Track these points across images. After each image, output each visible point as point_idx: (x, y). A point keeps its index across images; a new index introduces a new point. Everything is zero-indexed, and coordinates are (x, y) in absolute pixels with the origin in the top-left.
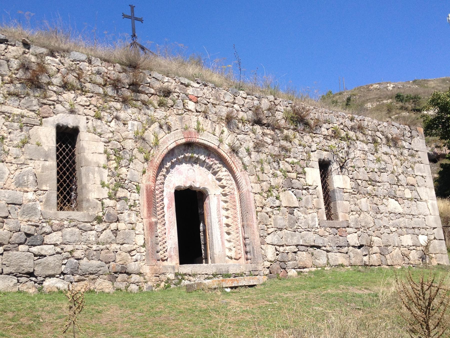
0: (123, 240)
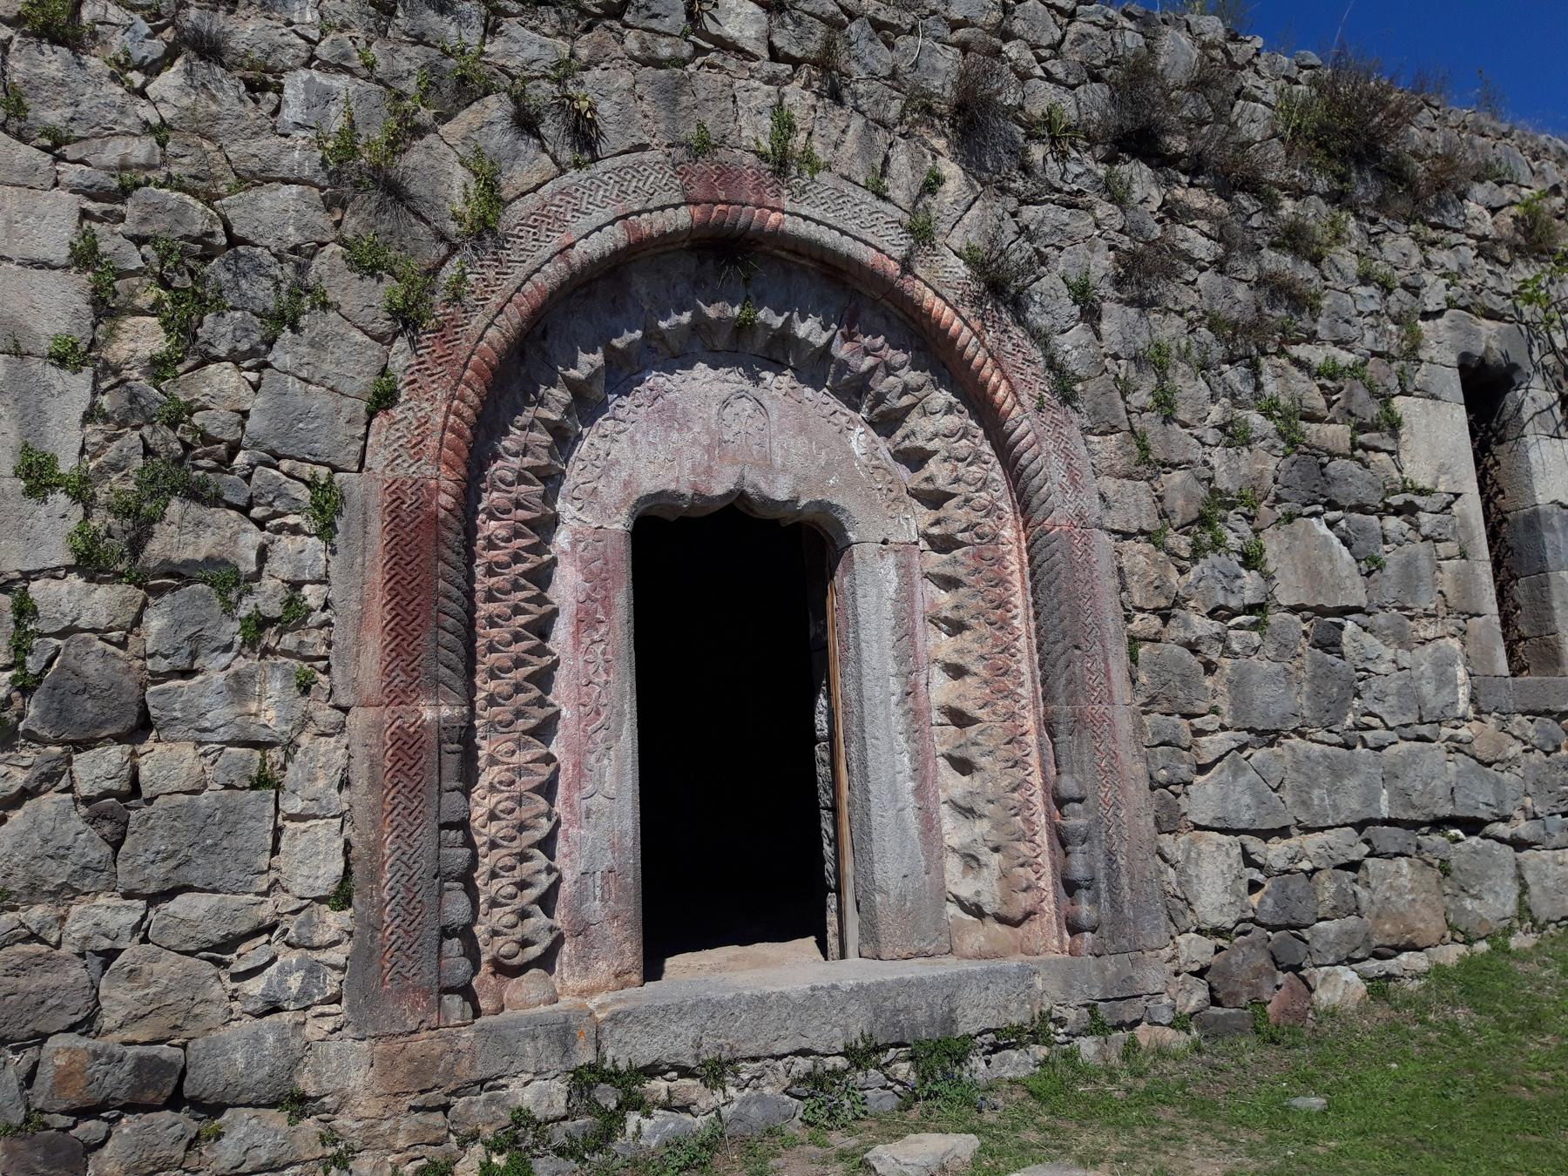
0: (172, 863)
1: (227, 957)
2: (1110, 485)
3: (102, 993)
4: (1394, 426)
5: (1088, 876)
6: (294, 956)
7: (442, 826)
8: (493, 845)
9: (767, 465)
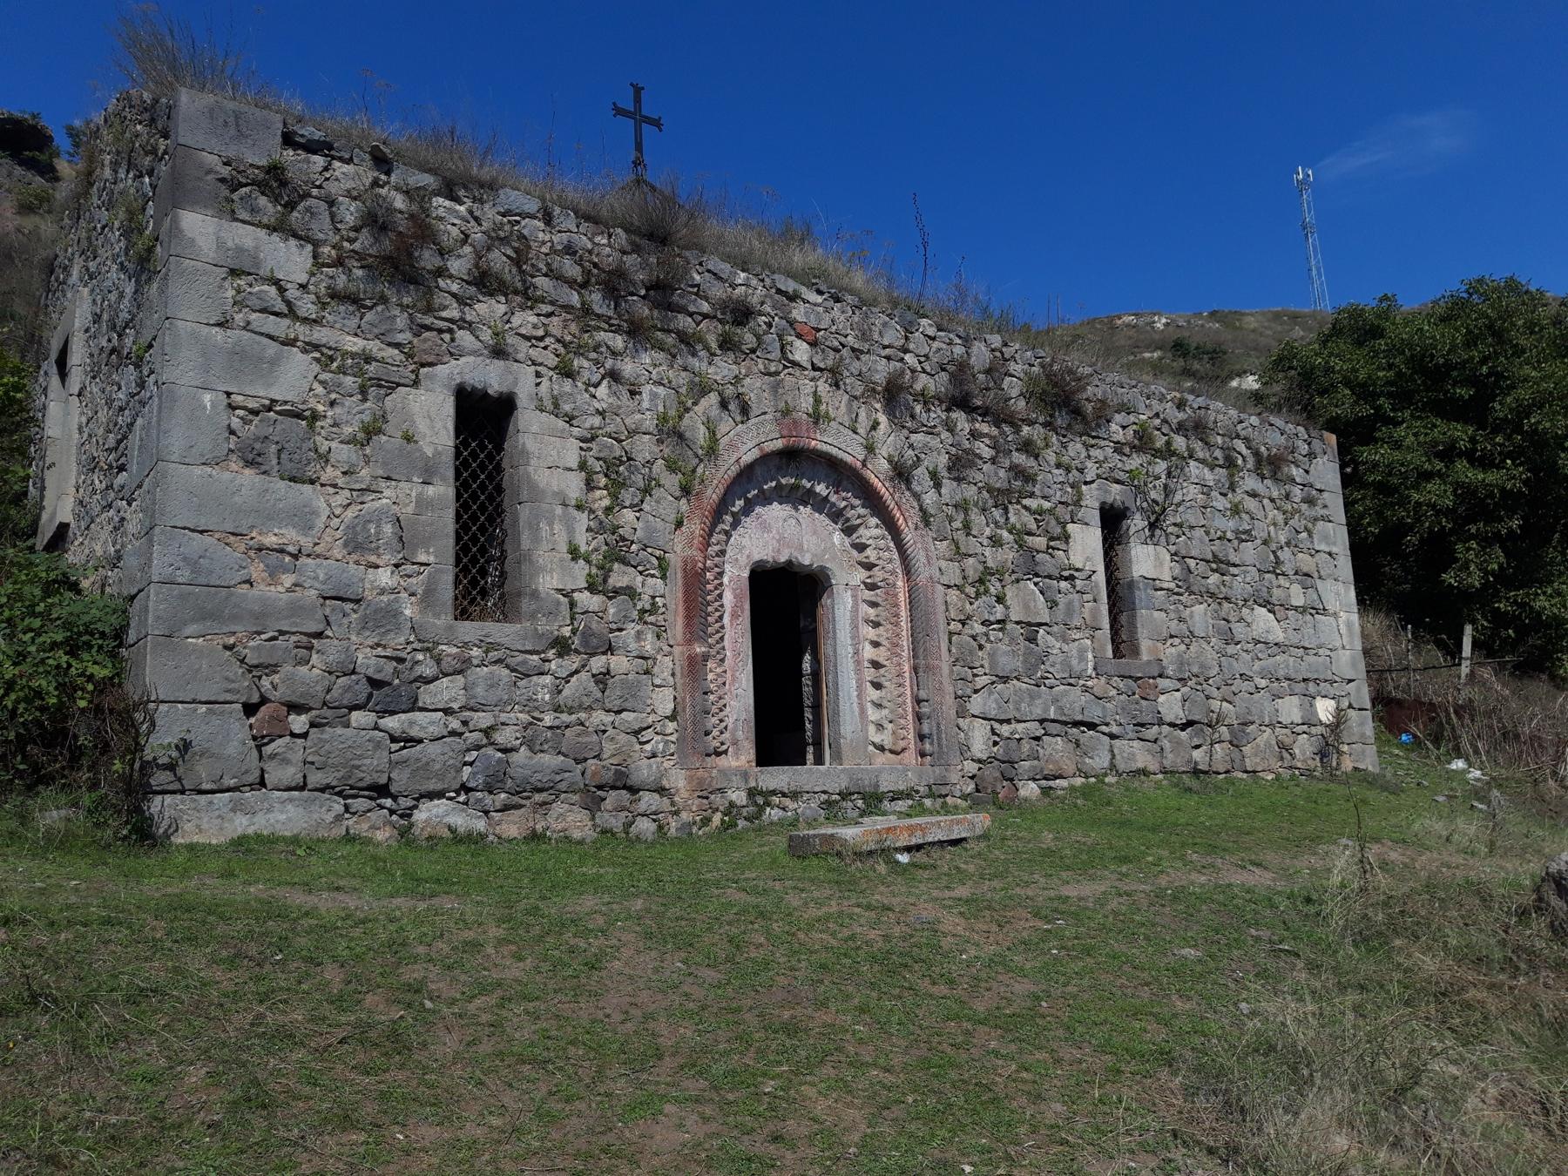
2: (943, 564)
4: (1066, 538)
6: (659, 737)
9: (801, 548)
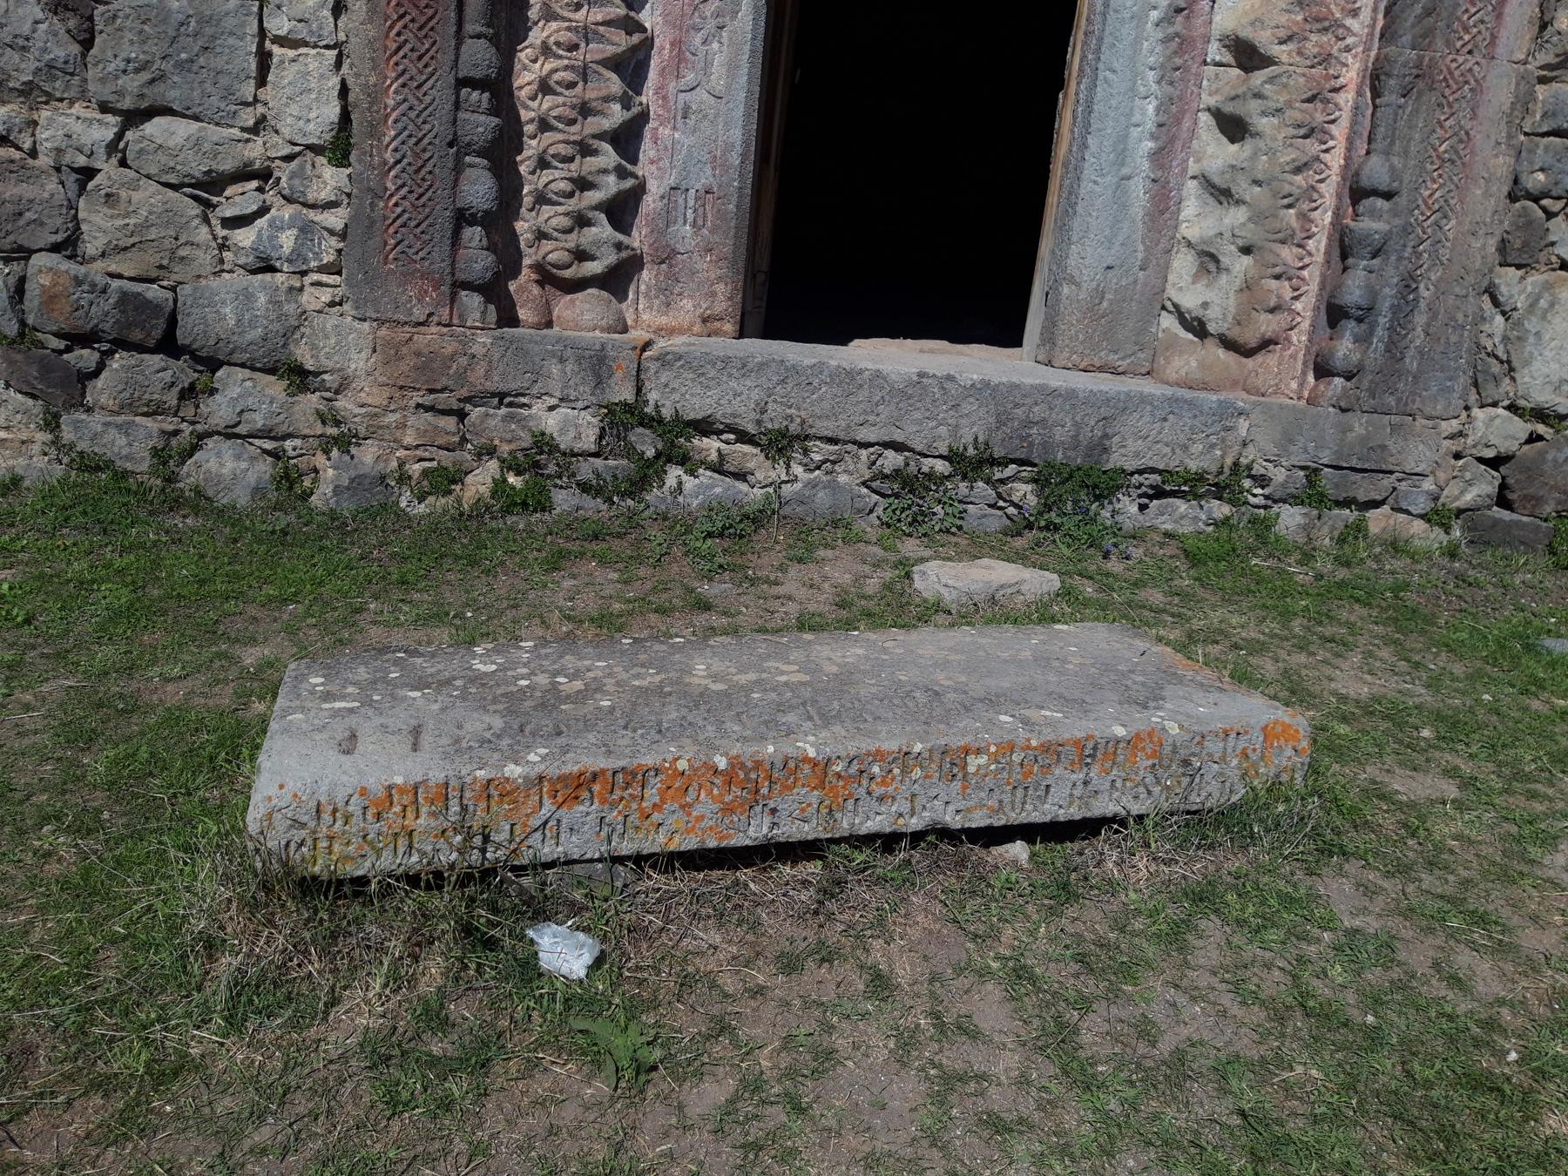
0: (145, 76)
1: (215, 199)
3: (81, 215)
5: (1364, 303)
6: (288, 212)
7: (462, 83)
8: (544, 125)
